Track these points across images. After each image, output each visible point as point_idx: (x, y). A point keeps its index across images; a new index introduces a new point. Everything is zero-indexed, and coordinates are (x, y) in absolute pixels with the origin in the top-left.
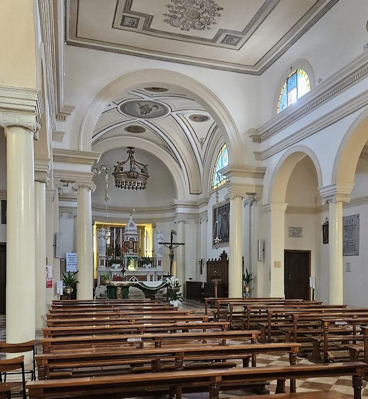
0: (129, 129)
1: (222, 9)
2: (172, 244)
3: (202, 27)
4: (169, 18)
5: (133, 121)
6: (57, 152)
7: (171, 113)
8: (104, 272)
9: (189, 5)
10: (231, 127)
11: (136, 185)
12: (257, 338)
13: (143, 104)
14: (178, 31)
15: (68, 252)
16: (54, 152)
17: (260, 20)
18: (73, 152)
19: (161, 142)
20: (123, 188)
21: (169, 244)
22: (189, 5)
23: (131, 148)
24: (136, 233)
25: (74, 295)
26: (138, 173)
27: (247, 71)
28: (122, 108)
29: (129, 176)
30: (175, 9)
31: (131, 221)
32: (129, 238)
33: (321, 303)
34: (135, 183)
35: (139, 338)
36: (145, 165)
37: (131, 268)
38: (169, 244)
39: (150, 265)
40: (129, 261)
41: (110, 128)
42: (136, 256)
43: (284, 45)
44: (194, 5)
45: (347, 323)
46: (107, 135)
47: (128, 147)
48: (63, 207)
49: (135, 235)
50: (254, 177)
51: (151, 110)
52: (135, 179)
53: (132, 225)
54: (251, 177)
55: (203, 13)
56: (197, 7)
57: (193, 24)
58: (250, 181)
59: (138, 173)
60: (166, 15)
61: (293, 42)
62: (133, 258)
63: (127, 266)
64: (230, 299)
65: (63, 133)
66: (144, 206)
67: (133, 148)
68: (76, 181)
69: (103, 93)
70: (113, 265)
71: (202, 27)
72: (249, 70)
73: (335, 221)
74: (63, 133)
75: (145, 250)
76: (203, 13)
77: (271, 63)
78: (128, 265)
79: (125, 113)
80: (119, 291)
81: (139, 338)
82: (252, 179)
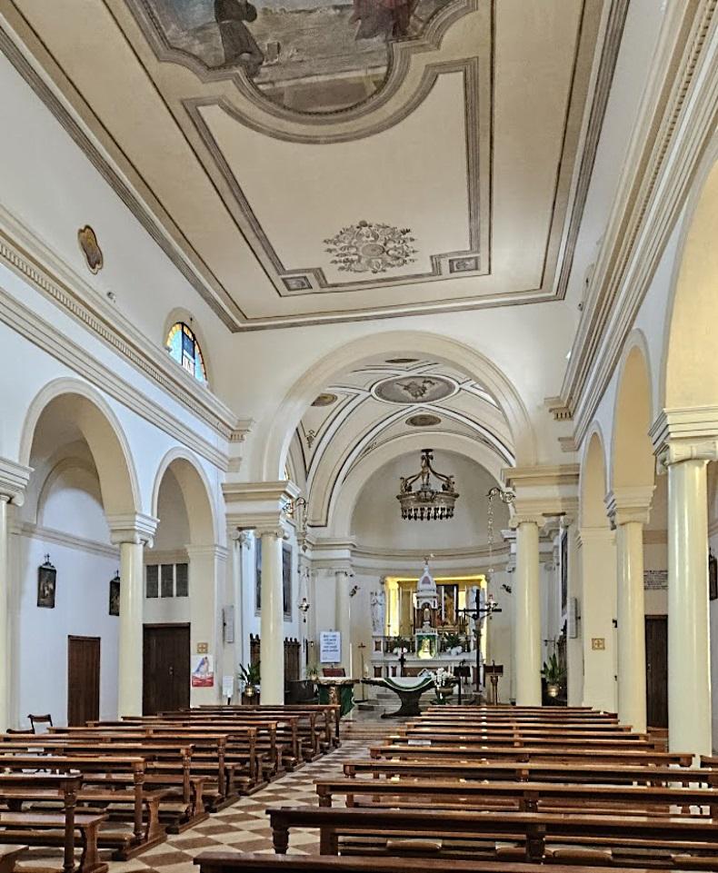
0: (413, 421)
1: (408, 231)
2: (478, 610)
3: (401, 261)
4: (343, 265)
5: (409, 410)
6: (228, 489)
7: (461, 386)
8: (379, 661)
9: (355, 240)
10: (513, 403)
11: (440, 512)
12: (188, 755)
13: (406, 383)
14: (369, 276)
15: (325, 630)
16: (223, 489)
17: (485, 226)
18: (249, 485)
19: (475, 435)
20: (425, 520)
21: (474, 610)
22: (355, 240)
23: (427, 451)
24: (435, 594)
25: (257, 696)
26: (433, 493)
27: (529, 299)
28: (379, 392)
29: (419, 500)
30: (340, 252)
31: (426, 574)
32: (421, 604)
33: (590, 708)
34: (430, 509)
35: (40, 747)
36: (448, 475)
37: (424, 655)
38: (474, 610)
39: (459, 649)
40: (420, 642)
41: (391, 419)
42: (432, 634)
43: (562, 250)
44: (364, 239)
45: (430, 743)
46: (379, 440)
47: (423, 451)
48: (319, 560)
49: (430, 597)
50: (559, 484)
51: (424, 389)
52: (430, 503)
53: (426, 581)
54: (553, 485)
55: (385, 244)
56: (369, 239)
57: (384, 261)
58: (554, 491)
59: (433, 493)
60: (336, 262)
61: (573, 239)
62: (428, 637)
63: (418, 651)
64: (570, 708)
65: (240, 459)
66: (470, 544)
67: (431, 450)
68: (257, 526)
69: (295, 390)
70: (395, 651)
71: (401, 261)
72: (530, 297)
73: (626, 556)
74: (240, 459)
75: (387, 623)
76: (385, 244)
77: (566, 272)
78: (419, 649)
79: (384, 398)
80: (333, 692)
81: (40, 747)
82: (556, 487)
